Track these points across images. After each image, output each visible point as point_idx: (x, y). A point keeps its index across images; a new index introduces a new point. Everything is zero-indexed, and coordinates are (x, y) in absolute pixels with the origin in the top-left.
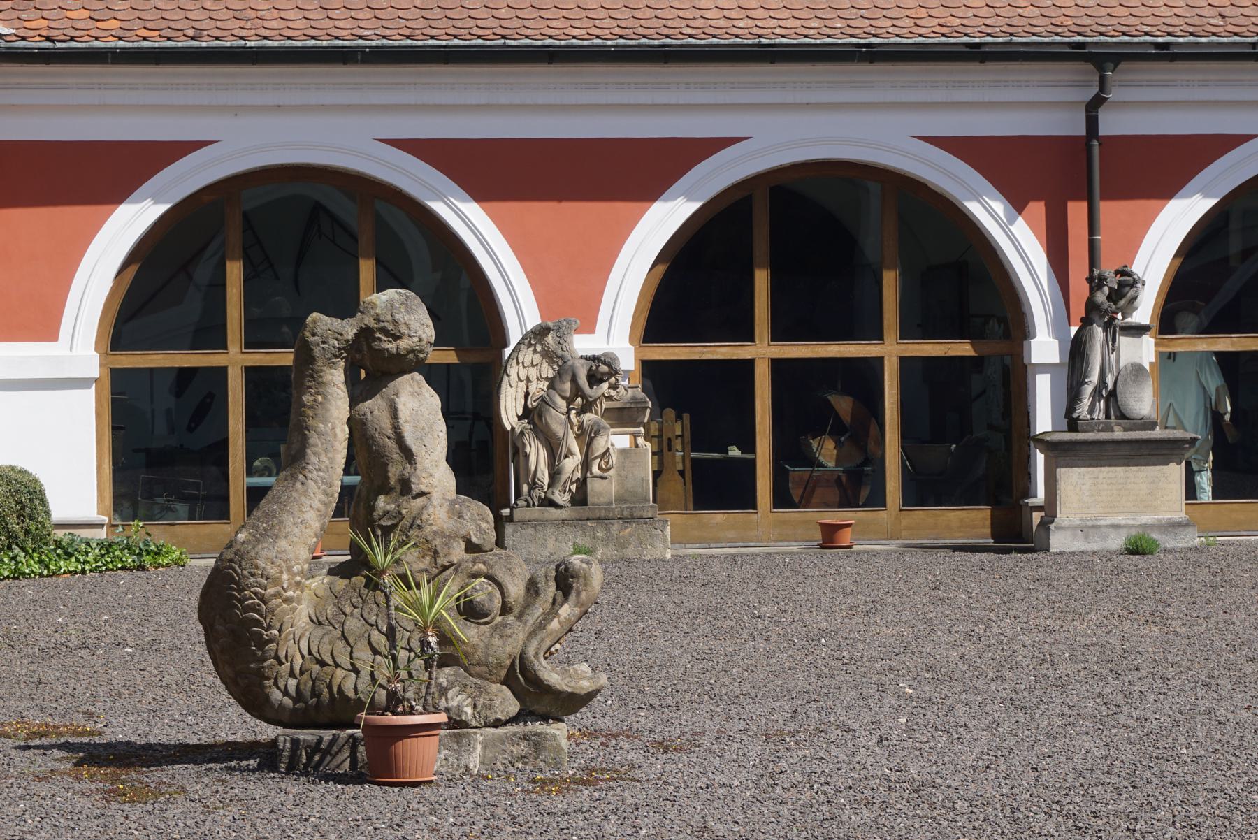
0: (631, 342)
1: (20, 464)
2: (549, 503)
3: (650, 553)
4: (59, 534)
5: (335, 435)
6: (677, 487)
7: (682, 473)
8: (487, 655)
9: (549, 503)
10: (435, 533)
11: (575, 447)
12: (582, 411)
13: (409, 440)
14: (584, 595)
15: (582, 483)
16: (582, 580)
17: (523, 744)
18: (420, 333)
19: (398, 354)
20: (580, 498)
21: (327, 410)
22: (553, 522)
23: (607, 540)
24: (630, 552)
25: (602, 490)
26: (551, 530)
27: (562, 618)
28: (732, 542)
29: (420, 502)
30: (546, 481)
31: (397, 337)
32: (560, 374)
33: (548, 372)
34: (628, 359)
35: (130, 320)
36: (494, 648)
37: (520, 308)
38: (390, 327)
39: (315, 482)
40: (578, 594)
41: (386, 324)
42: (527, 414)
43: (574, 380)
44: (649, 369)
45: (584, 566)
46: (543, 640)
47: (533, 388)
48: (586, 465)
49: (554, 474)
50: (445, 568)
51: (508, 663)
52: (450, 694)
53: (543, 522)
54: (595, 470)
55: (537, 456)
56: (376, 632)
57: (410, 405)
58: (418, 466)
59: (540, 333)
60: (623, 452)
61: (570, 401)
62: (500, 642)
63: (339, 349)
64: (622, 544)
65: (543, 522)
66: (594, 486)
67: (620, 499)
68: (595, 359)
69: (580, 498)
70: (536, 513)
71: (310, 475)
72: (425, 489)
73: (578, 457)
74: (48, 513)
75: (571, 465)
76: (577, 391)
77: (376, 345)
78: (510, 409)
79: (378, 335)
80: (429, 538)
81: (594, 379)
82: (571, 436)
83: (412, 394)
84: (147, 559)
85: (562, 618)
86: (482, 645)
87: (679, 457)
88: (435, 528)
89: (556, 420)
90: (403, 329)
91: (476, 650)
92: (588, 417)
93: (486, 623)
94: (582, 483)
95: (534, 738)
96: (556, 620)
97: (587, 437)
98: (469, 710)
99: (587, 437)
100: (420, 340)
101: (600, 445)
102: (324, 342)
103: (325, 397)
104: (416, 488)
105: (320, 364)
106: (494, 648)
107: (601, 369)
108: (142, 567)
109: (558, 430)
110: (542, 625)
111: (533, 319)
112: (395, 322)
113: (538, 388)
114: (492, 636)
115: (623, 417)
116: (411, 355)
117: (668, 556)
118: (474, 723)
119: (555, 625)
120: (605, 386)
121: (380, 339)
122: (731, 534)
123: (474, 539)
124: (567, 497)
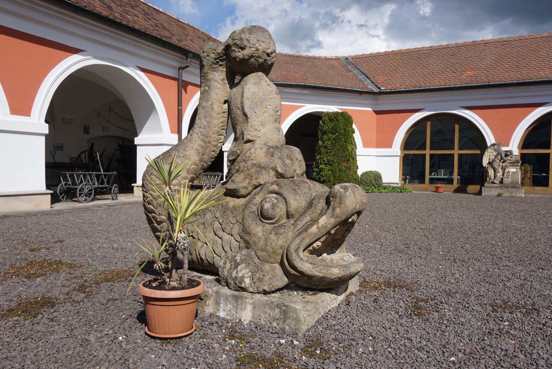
0: (518, 148)
1: (377, 171)
2: (493, 183)
3: (519, 195)
4: (384, 185)
5: (213, 109)
6: (528, 181)
7: (530, 178)
8: (266, 245)
9: (493, 183)
10: (254, 165)
11: (501, 170)
12: (503, 162)
13: (247, 110)
14: (338, 210)
15: (502, 179)
16: (338, 200)
17: (277, 311)
18: (257, 45)
19: (244, 59)
20: (501, 182)
21: (210, 94)
22: (494, 187)
23: (507, 192)
24: (513, 195)
25: (507, 181)
26: (493, 189)
27: (320, 225)
28: (542, 194)
29: (248, 145)
30: (493, 178)
31: (243, 49)
32: (498, 154)
33: (495, 154)
34: (516, 152)
35: (407, 144)
36: (271, 241)
37: (490, 139)
38: (239, 43)
39: (197, 134)
40: (334, 209)
41: (236, 41)
42: (489, 163)
43: (501, 156)
44: (523, 156)
45: (342, 190)
46: (304, 239)
47: (491, 158)
48: (503, 175)
49: (495, 177)
50: (256, 187)
51: (280, 251)
52: (240, 268)
53: (492, 187)
54: (505, 176)
55: (491, 172)
56: (217, 222)
57: (252, 90)
58: (249, 124)
59: (493, 145)
60: (513, 172)
61: (500, 161)
62: (275, 238)
63: (215, 59)
64: (511, 193)
65: (492, 187)
66: (505, 180)
67: (511, 183)
68: (507, 151)
69: (501, 182)
70: (490, 185)
71: (195, 130)
72: (252, 139)
73: (501, 173)
74: (381, 180)
75: (500, 174)
76: (502, 158)
77: (233, 55)
78: (485, 162)
79: (233, 48)
80: (249, 168)
81: (506, 155)
82: (500, 168)
83: (255, 84)
84: (403, 190)
85: (320, 225)
86: (263, 238)
87: (529, 175)
88: (255, 162)
89: (496, 165)
90: (245, 43)
91: (260, 241)
92: (504, 164)
93: (272, 224)
94: (502, 179)
95: (284, 308)
96: (315, 226)
97: (504, 169)
98: (247, 281)
99: (504, 169)
100: (257, 50)
101: (507, 170)
102: (208, 56)
103: (209, 87)
104: (246, 137)
105: (206, 69)
106: (271, 241)
107: (508, 154)
108: (401, 192)
109: (496, 167)
110: (306, 229)
111: (493, 141)
112: (241, 39)
113: (492, 157)
114: (271, 233)
115: (513, 164)
116: (252, 60)
117: (523, 196)
118: (251, 290)
119: (314, 229)
120: (509, 157)
121: (234, 50)
122: (541, 192)
123: (279, 170)
124: (498, 182)
